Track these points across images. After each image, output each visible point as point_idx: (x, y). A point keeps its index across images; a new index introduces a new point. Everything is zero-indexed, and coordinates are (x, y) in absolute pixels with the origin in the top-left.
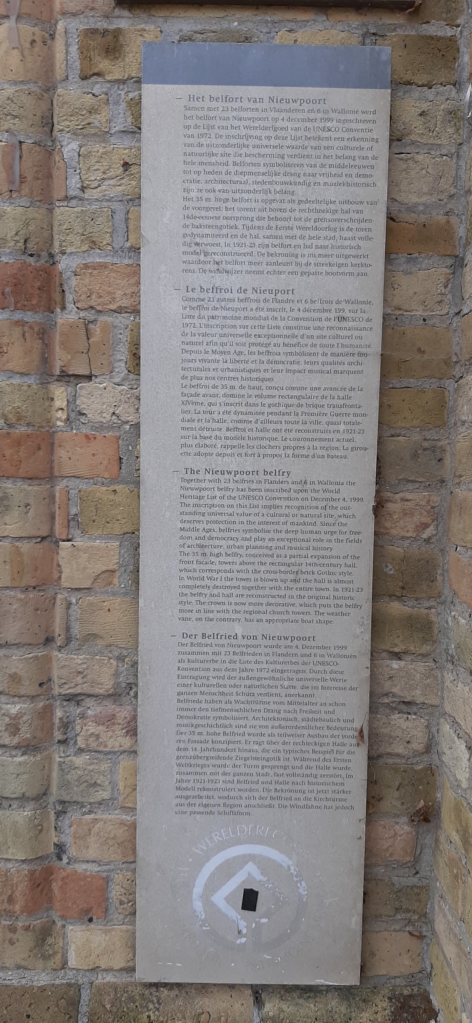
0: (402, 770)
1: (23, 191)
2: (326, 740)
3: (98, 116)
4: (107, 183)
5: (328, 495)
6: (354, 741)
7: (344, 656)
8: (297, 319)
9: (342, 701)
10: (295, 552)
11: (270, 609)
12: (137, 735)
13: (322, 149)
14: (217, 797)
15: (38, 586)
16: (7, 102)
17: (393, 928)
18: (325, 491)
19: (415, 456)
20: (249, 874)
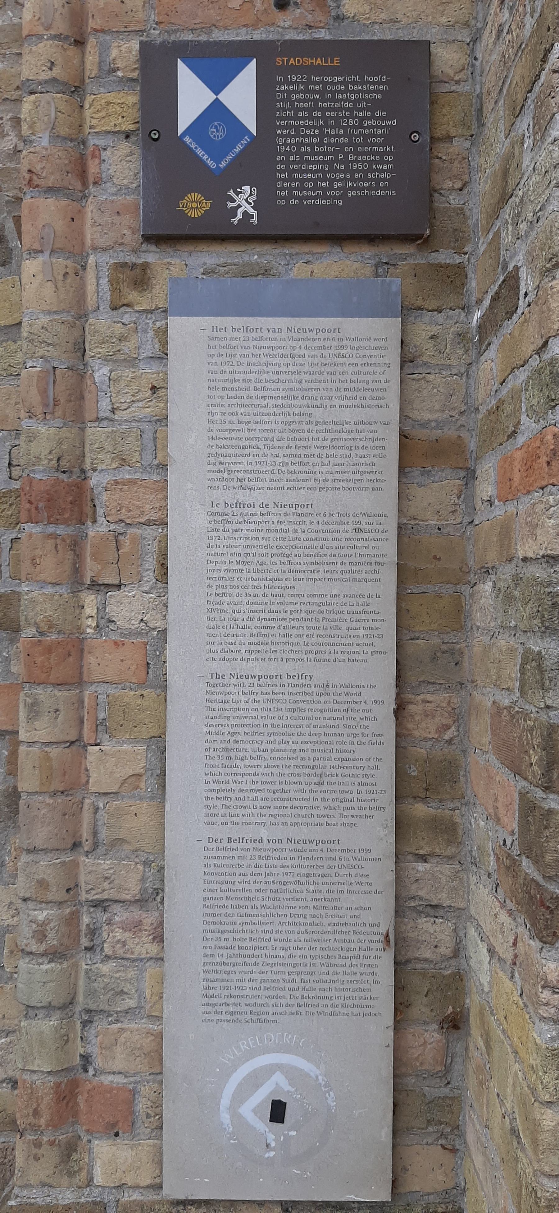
0: (430, 975)
1: (56, 413)
2: (352, 946)
3: (128, 343)
4: (135, 405)
5: (350, 698)
6: (380, 946)
7: (369, 859)
8: (316, 531)
9: (368, 905)
10: (318, 755)
11: (294, 812)
12: (163, 942)
13: (338, 373)
14: (243, 1005)
15: (66, 791)
16: (41, 331)
17: (425, 1141)
18: (347, 694)
19: (434, 658)
20: (277, 1084)
